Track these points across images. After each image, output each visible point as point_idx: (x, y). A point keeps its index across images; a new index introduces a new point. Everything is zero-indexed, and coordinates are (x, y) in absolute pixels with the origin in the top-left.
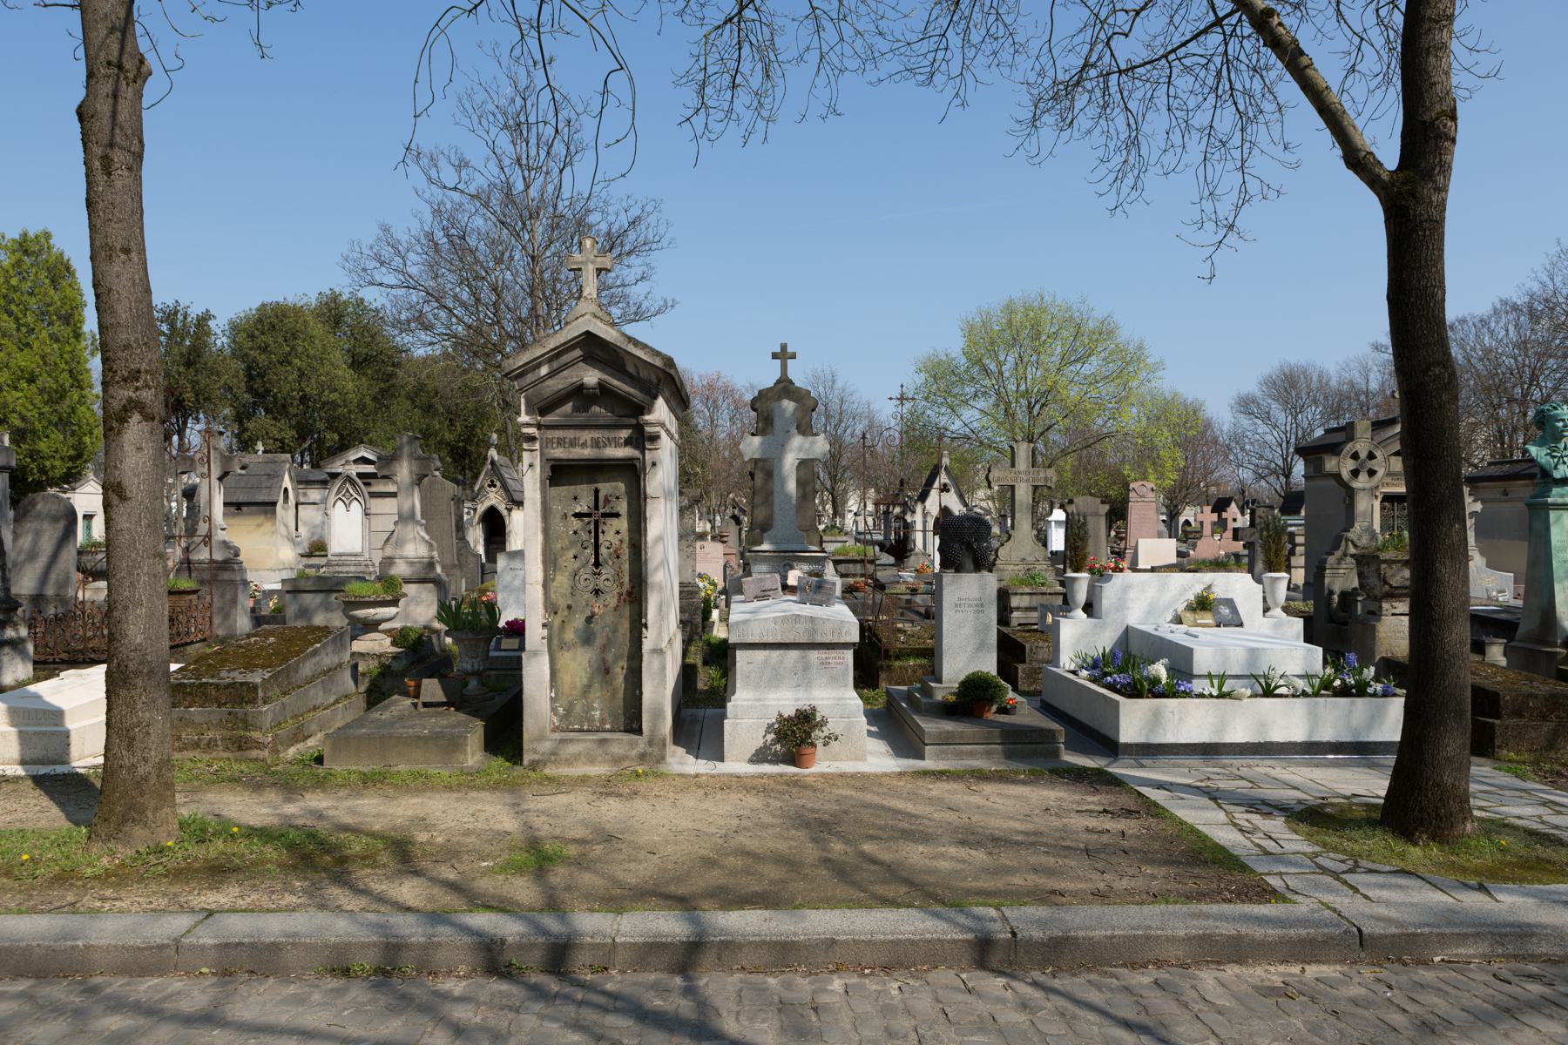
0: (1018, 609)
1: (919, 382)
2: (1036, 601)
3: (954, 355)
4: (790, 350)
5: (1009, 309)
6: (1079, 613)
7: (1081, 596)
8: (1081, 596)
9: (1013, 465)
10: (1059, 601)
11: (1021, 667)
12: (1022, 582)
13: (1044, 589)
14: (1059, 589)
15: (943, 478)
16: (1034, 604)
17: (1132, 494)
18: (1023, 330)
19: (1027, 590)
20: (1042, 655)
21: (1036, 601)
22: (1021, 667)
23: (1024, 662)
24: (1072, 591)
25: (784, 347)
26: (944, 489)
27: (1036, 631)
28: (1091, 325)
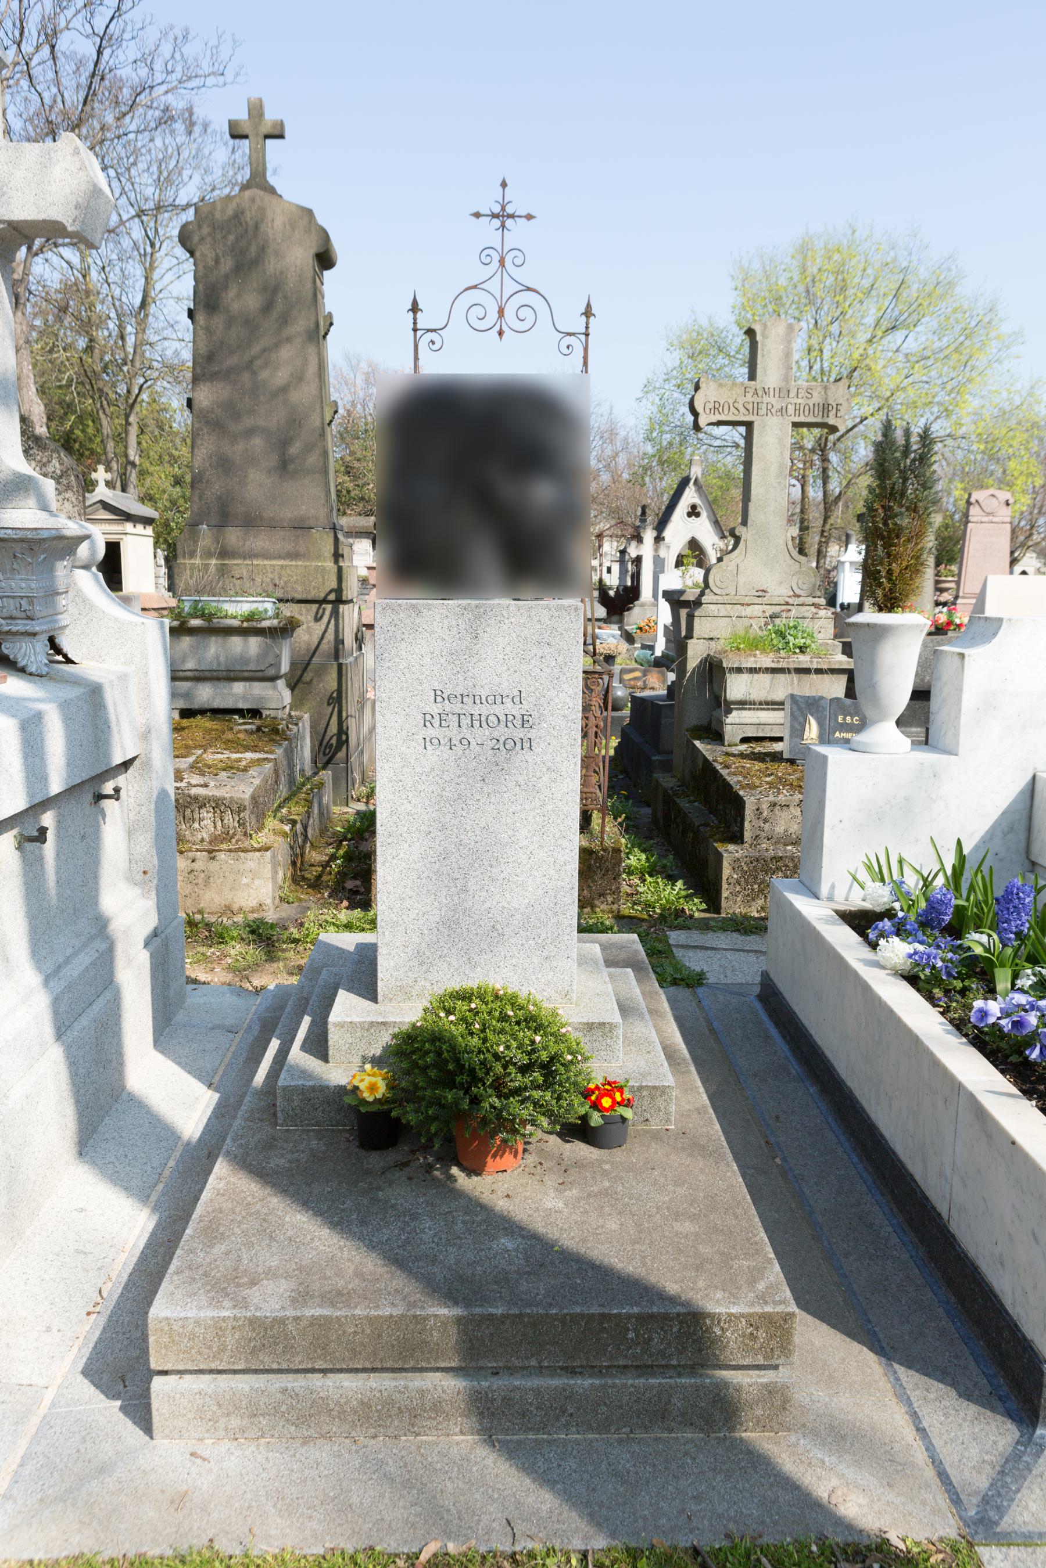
0: (743, 704)
1: (670, 366)
2: (781, 688)
3: (722, 324)
4: (271, 115)
5: (804, 250)
6: (887, 736)
7: (897, 674)
8: (897, 686)
9: (752, 376)
10: (836, 687)
11: (730, 853)
12: (755, 645)
13: (803, 660)
14: (841, 660)
15: (690, 496)
16: (779, 695)
17: (974, 511)
18: (820, 286)
19: (766, 661)
20: (786, 823)
21: (781, 688)
22: (730, 853)
23: (737, 838)
24: (872, 663)
25: (256, 110)
26: (694, 512)
27: (776, 757)
28: (923, 273)
